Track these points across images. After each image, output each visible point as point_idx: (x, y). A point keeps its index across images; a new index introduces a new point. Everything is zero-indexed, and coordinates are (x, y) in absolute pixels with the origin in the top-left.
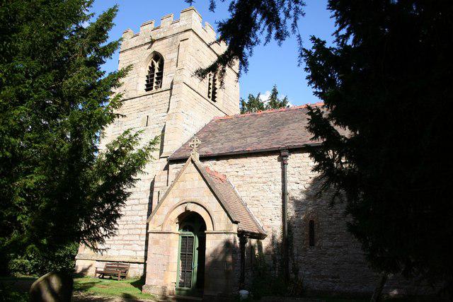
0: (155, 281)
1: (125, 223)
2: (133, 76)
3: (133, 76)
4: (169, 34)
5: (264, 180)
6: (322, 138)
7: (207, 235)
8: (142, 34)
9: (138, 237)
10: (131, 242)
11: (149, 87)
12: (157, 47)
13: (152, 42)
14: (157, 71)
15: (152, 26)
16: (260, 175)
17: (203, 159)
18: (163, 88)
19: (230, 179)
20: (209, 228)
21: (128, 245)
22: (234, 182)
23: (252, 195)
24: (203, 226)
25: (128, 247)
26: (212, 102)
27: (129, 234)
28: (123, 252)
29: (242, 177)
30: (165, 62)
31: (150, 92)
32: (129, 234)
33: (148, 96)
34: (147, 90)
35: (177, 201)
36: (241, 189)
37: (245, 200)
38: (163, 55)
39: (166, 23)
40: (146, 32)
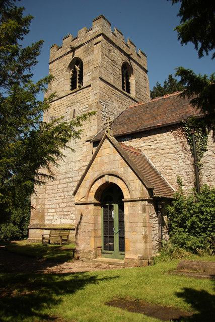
0: (83, 246)
1: (63, 197)
2: (61, 80)
3: (61, 80)
4: (85, 41)
5: (175, 150)
6: (197, 94)
7: (125, 203)
8: (65, 46)
9: (49, 211)
10: (69, 213)
11: (73, 86)
12: (78, 54)
13: (73, 50)
14: (78, 73)
15: (70, 39)
16: (171, 146)
17: (120, 138)
18: (84, 85)
19: (145, 153)
20: (126, 196)
21: (67, 215)
22: (147, 155)
23: (165, 165)
24: (121, 195)
25: (67, 217)
26: (127, 93)
27: (66, 206)
28: (64, 221)
29: (155, 149)
30: (84, 64)
31: (74, 91)
32: (66, 206)
33: (74, 94)
34: (72, 89)
35: (97, 175)
36: (154, 160)
37: (158, 170)
38: (82, 58)
39: (82, 33)
40: (67, 43)
